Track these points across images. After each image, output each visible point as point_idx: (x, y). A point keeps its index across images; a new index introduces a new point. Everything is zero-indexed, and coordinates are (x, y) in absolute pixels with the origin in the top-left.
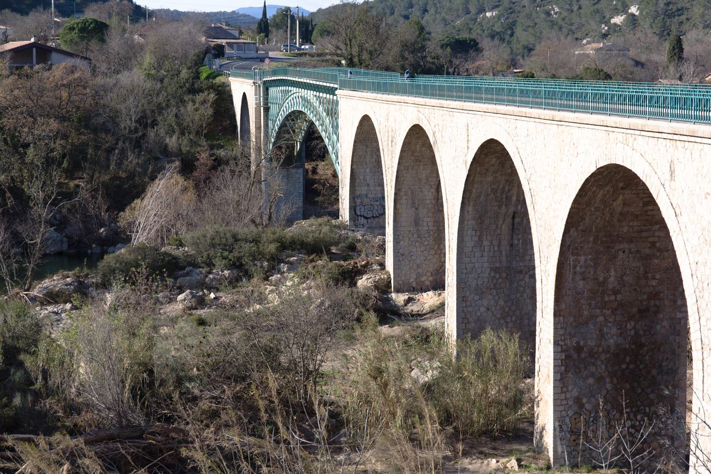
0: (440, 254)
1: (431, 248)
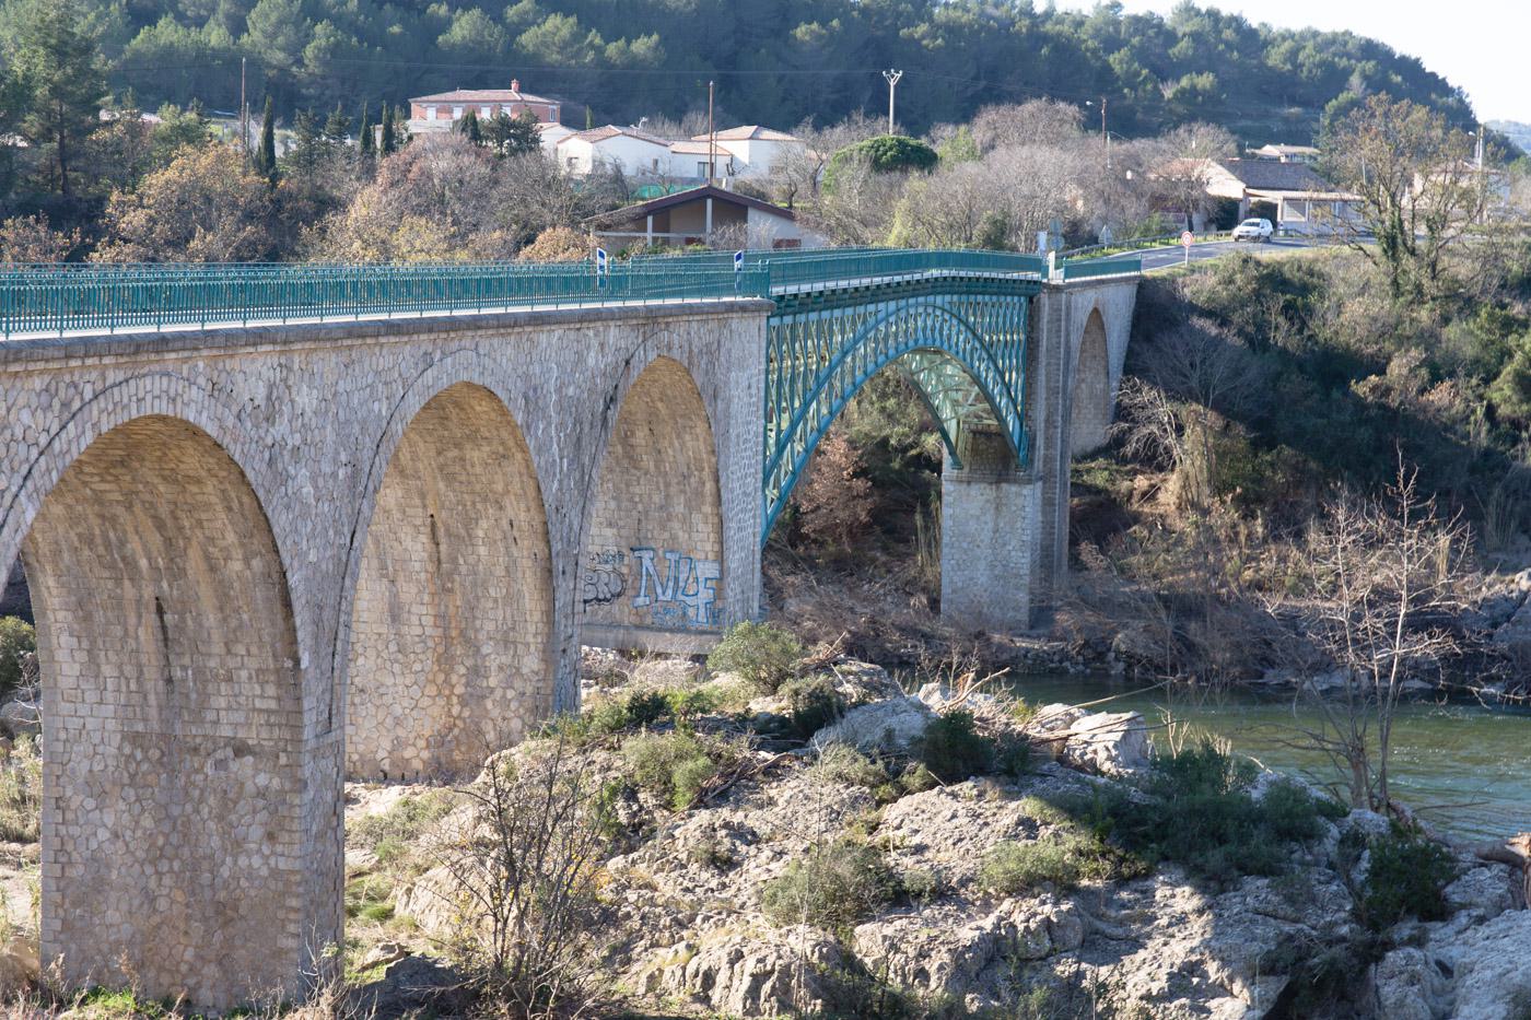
0: (448, 697)
1: (428, 681)
